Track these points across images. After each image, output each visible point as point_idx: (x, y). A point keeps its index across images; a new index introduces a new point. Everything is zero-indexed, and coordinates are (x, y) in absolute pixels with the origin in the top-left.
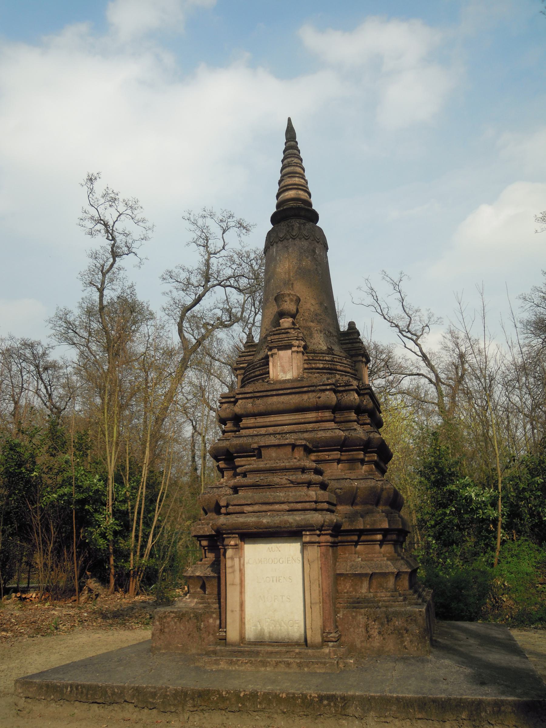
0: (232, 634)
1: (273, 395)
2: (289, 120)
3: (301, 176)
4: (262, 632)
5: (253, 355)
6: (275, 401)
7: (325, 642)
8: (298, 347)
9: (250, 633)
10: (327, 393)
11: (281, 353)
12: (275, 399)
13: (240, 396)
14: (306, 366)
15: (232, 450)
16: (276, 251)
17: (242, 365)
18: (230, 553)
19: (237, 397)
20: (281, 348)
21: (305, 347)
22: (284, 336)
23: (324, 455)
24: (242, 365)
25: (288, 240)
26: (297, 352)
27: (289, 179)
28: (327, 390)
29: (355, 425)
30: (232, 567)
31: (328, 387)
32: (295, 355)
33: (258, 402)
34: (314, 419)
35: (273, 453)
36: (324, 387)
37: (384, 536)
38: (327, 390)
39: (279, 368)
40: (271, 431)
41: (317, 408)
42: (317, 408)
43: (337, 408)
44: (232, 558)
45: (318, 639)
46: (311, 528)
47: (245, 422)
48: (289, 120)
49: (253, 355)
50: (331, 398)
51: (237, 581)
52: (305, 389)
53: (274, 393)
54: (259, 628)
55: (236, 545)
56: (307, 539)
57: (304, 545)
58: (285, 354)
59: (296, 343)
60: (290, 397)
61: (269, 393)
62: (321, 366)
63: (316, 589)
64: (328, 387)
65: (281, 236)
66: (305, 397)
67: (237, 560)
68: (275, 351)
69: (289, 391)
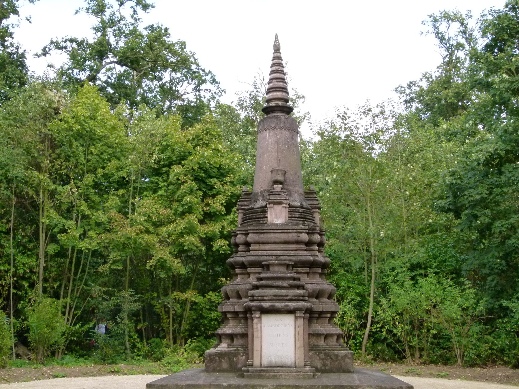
0: (257, 362)
1: (271, 233)
2: (276, 35)
3: (282, 81)
4: (271, 361)
5: (250, 201)
6: (271, 237)
7: (305, 365)
8: (286, 204)
9: (265, 362)
10: (303, 234)
11: (276, 207)
12: (272, 235)
13: (251, 231)
14: (290, 216)
15: (246, 263)
16: (269, 135)
17: (243, 207)
18: (255, 321)
19: (249, 231)
20: (275, 204)
21: (289, 204)
22: (277, 196)
23: (300, 270)
24: (243, 207)
25: (277, 129)
26: (286, 207)
27: (276, 83)
28: (303, 232)
29: (317, 254)
30: (257, 328)
31: (304, 231)
32: (284, 209)
33: (261, 236)
34: (295, 249)
35: (276, 269)
36: (301, 231)
37: (319, 315)
38: (303, 232)
39: (274, 216)
40: (270, 254)
41: (297, 242)
42: (297, 242)
43: (309, 244)
44: (257, 324)
45: (302, 364)
46: (300, 309)
47: (252, 247)
48: (276, 35)
49: (250, 201)
50: (305, 237)
51: (259, 335)
52: (290, 231)
53: (272, 231)
54: (270, 359)
55: (259, 317)
56: (297, 315)
57: (296, 318)
58: (278, 208)
59: (285, 201)
60: (281, 234)
61: (268, 231)
62: (298, 216)
63: (302, 339)
64: (304, 231)
65: (273, 126)
66: (290, 235)
67: (259, 325)
68: (272, 205)
69: (280, 231)
